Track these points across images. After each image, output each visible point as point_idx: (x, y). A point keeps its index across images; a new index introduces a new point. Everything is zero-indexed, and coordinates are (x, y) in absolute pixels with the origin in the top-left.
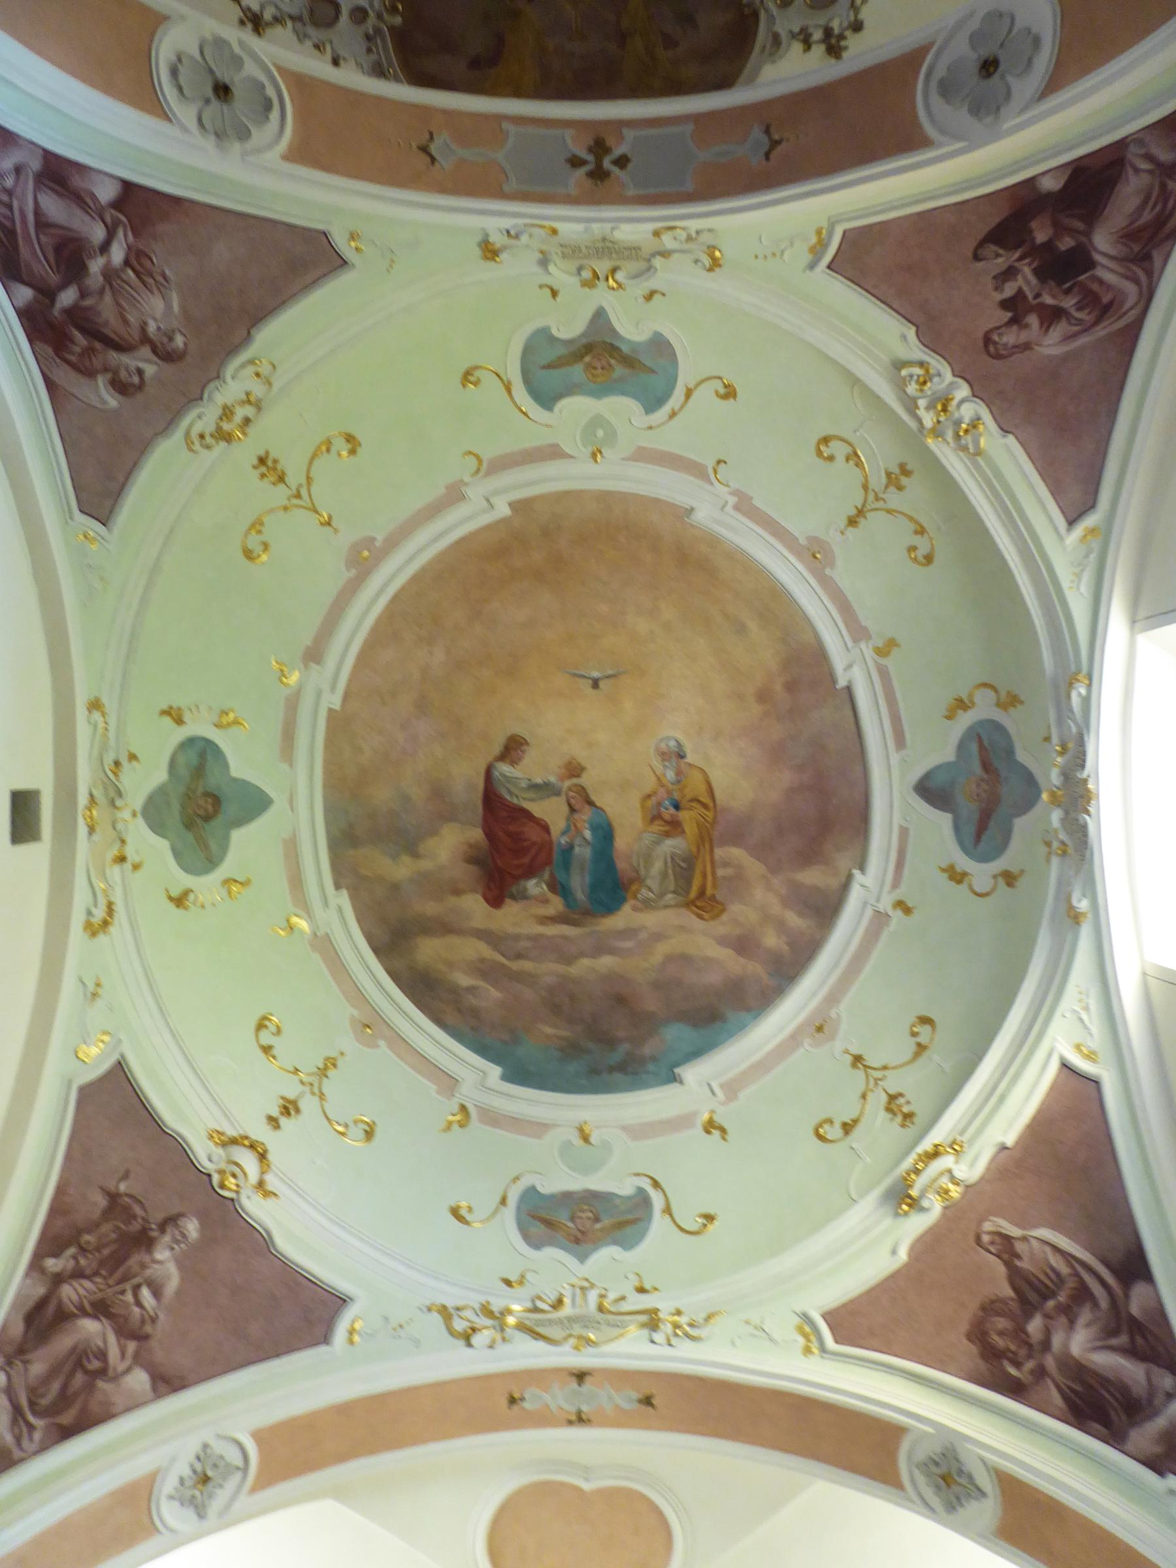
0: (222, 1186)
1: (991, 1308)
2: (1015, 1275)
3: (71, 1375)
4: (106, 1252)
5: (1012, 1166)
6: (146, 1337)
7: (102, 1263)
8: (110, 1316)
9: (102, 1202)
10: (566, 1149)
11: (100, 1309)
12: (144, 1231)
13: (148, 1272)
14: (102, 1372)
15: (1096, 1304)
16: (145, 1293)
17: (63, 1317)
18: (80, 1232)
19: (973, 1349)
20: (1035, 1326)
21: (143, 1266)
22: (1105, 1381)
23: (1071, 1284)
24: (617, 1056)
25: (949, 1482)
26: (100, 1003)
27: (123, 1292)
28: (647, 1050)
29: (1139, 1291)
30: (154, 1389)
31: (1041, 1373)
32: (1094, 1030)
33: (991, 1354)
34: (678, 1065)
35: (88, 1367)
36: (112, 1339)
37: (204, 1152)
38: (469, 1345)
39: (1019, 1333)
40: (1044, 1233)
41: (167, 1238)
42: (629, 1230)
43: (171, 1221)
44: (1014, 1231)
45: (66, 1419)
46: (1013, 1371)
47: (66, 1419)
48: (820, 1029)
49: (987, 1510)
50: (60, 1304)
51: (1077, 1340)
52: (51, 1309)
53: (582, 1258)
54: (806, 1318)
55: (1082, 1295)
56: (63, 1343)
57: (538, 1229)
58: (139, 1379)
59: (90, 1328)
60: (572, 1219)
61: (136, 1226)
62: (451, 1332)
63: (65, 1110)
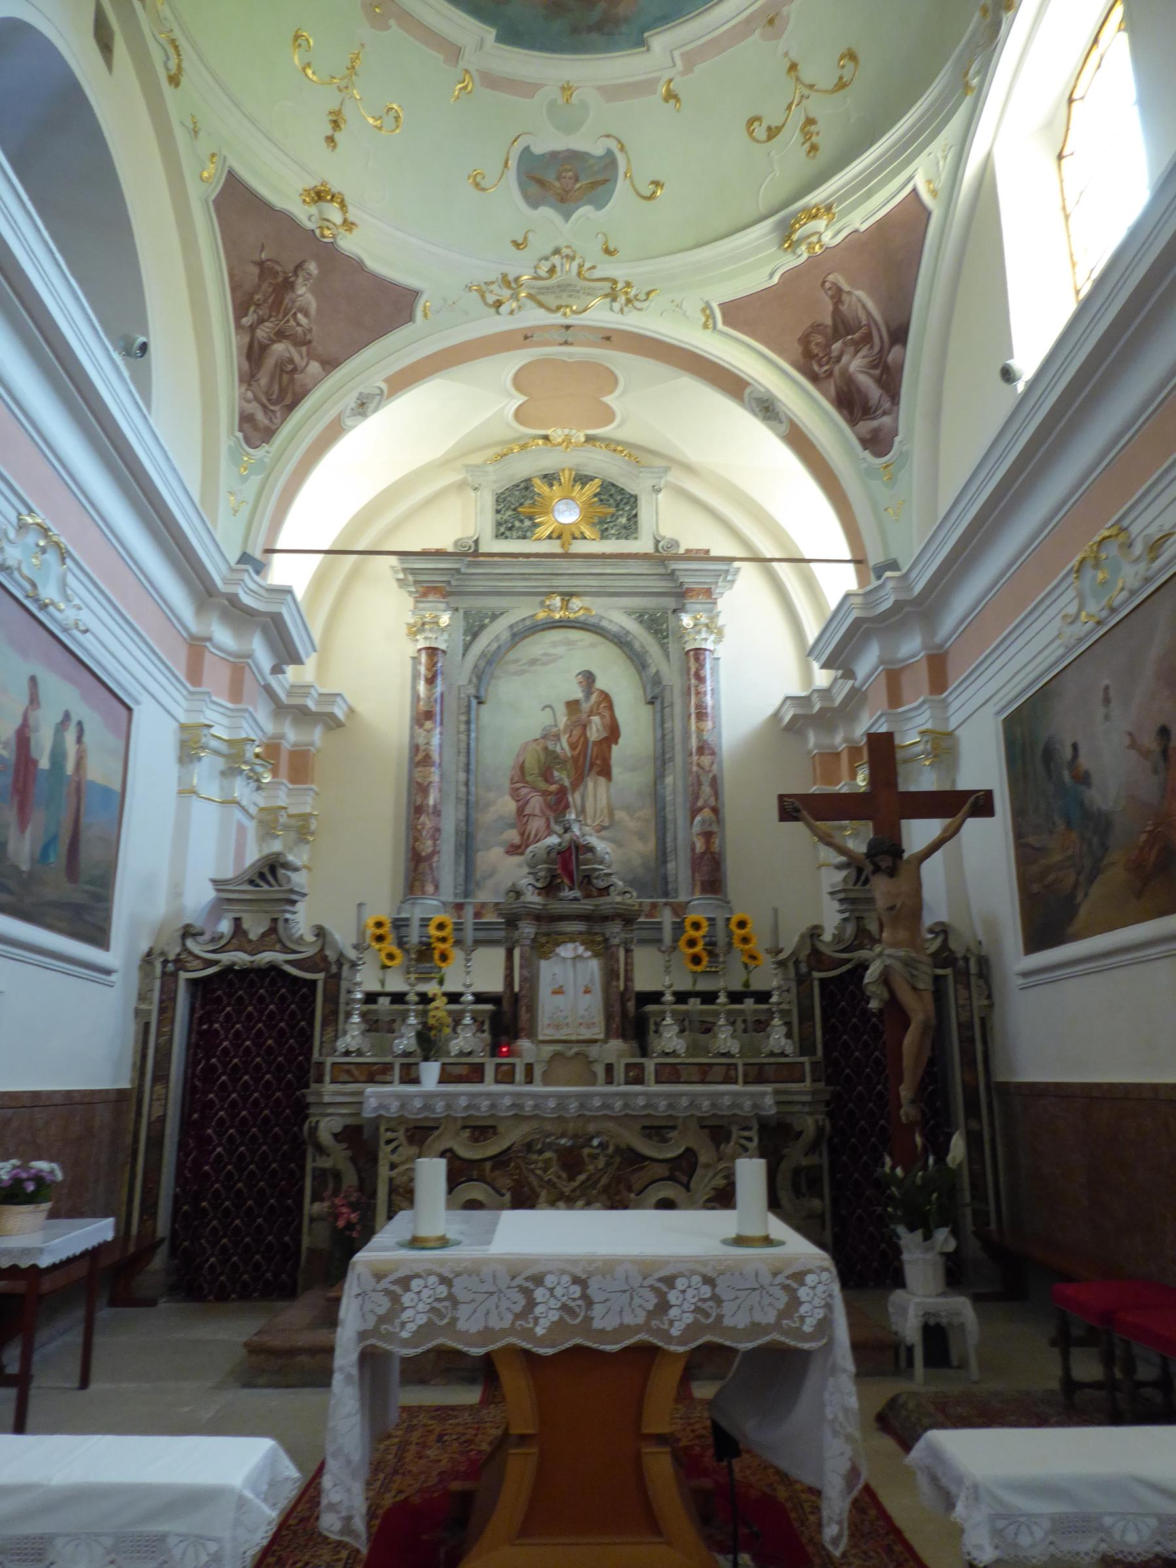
0: (323, 236)
1: (817, 328)
2: (836, 312)
3: (281, 376)
4: (270, 301)
5: (857, 244)
6: (310, 342)
7: (271, 310)
8: (287, 337)
9: (255, 270)
10: (552, 105)
11: (281, 335)
12: (286, 279)
13: (298, 304)
14: (295, 370)
15: (872, 347)
16: (299, 316)
17: (264, 348)
18: (252, 295)
19: (800, 349)
20: (837, 346)
21: (294, 302)
22: (859, 391)
23: (863, 330)
24: (596, 14)
25: (767, 409)
26: (202, 134)
27: (288, 321)
28: (621, 10)
29: (897, 349)
30: (324, 369)
31: (830, 374)
32: (943, 177)
33: (808, 355)
34: (648, 29)
35: (287, 369)
36: (292, 349)
37: (304, 214)
38: (498, 313)
39: (827, 346)
40: (860, 293)
41: (300, 280)
42: (600, 189)
43: (299, 267)
44: (846, 288)
45: (288, 401)
46: (816, 368)
47: (288, 401)
48: (771, 22)
49: (784, 428)
50: (260, 343)
51: (856, 365)
52: (256, 345)
53: (567, 216)
54: (708, 306)
55: (867, 339)
56: (270, 362)
57: (534, 189)
58: (314, 367)
59: (279, 348)
60: (559, 178)
61: (280, 279)
62: (486, 304)
63: (213, 225)
